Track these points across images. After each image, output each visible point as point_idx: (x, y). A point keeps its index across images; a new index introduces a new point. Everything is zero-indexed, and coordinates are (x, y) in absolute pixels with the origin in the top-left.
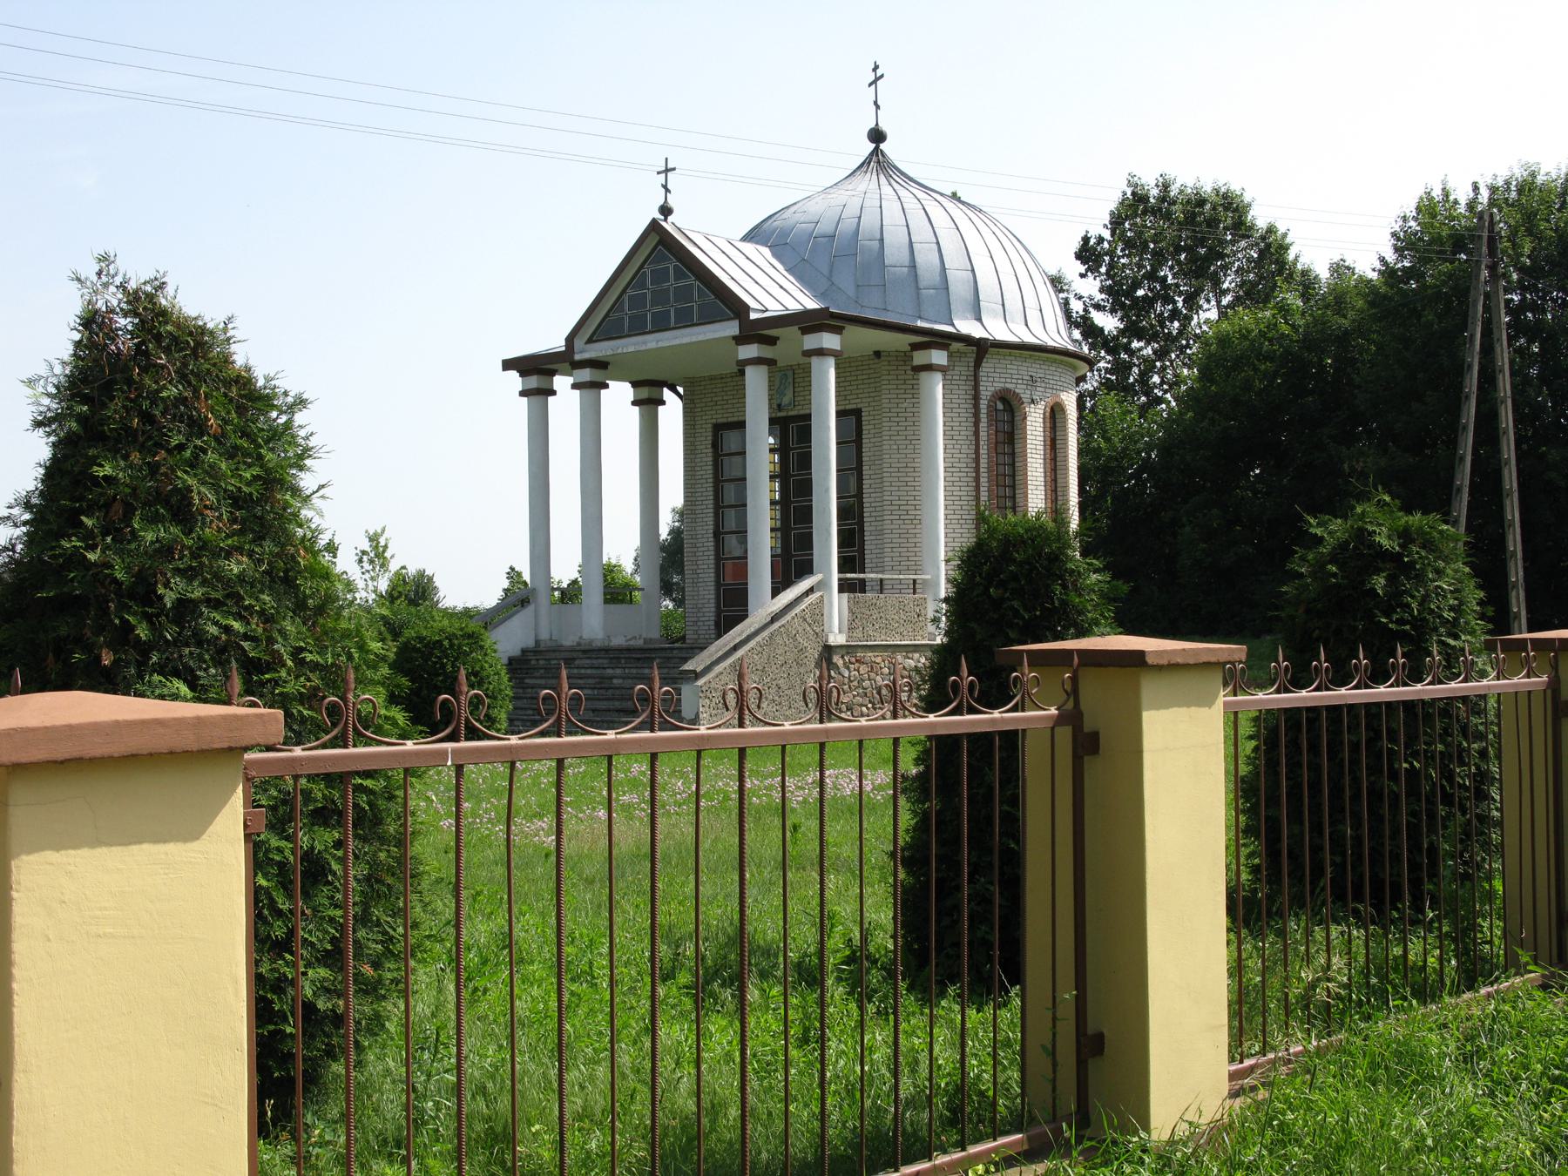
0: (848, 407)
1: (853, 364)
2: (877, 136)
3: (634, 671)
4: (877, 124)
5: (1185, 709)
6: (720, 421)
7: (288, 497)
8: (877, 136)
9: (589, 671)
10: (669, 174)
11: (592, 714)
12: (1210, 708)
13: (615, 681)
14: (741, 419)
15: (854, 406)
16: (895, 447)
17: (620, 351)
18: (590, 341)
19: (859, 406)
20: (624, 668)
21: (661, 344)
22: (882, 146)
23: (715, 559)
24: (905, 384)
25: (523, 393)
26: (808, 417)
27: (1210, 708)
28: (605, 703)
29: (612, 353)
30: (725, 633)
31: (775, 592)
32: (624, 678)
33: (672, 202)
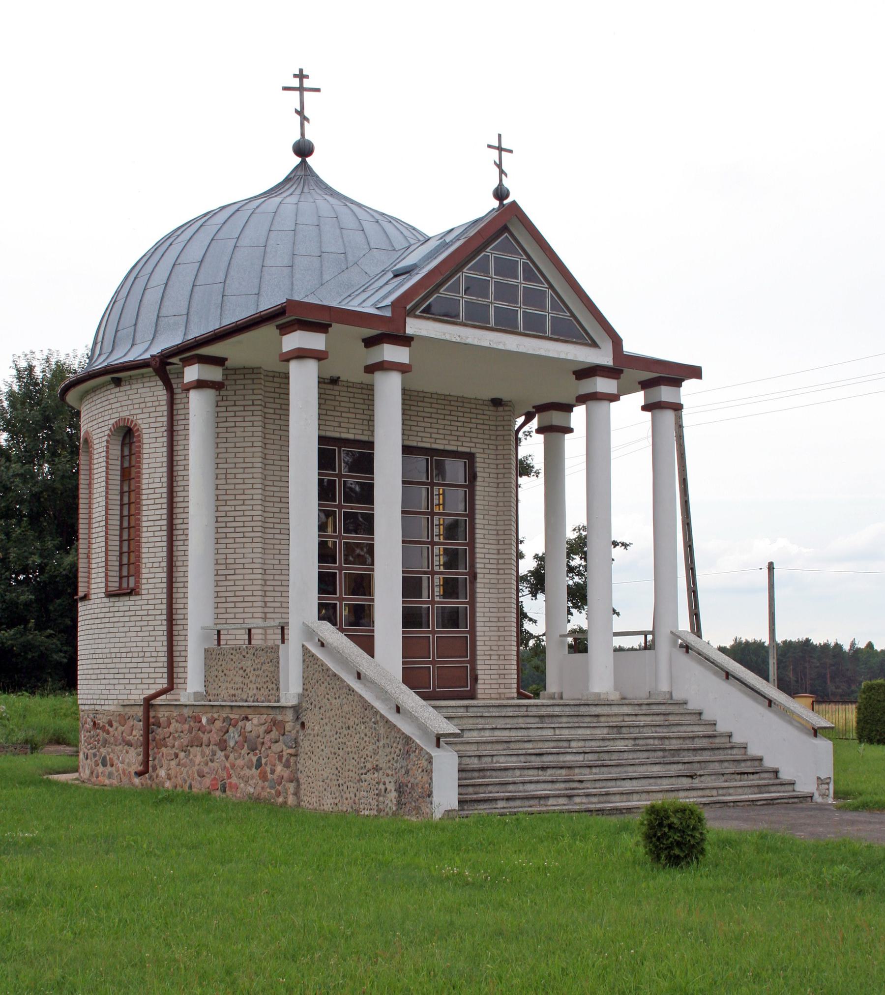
0: (461, 449)
2: (303, 149)
4: (303, 134)
5: (817, 640)
7: (56, 542)
8: (303, 149)
10: (298, 93)
12: (808, 641)
14: (371, 439)
15: (467, 450)
19: (473, 450)
22: (308, 160)
25: (645, 408)
26: (370, 445)
27: (808, 641)
30: (417, 693)
31: (367, 645)
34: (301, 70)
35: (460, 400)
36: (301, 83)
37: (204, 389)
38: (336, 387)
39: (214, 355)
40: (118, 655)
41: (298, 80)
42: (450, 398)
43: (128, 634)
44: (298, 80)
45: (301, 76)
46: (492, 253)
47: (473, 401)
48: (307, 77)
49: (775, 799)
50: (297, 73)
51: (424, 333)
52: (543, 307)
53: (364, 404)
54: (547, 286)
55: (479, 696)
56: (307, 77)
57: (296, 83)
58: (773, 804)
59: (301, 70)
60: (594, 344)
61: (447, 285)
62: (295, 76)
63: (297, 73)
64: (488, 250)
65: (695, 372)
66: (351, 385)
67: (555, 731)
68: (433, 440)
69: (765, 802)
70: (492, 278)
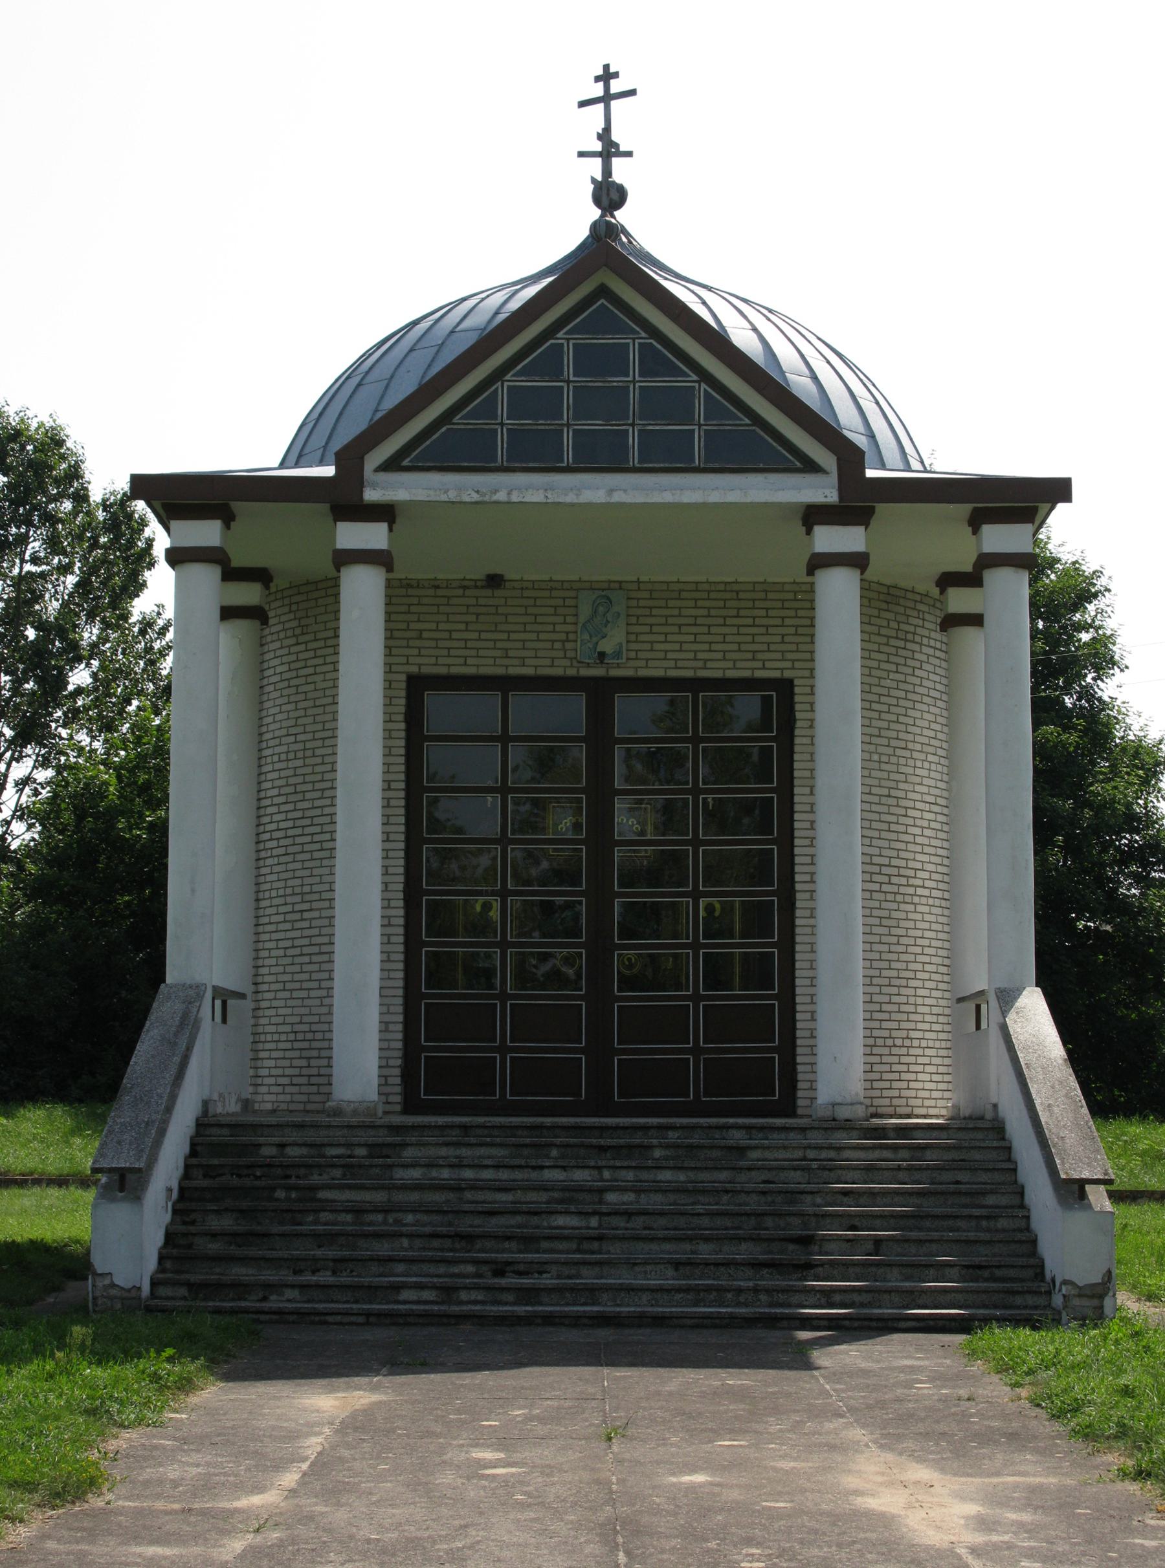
1: (771, 596)
3: (630, 1175)
6: (425, 670)
9: (488, 1174)
10: (614, 104)
11: (670, 1272)
13: (611, 1197)
15: (776, 674)
16: (876, 757)
17: (515, 498)
18: (392, 465)
19: (787, 674)
20: (599, 1168)
21: (617, 497)
23: (406, 943)
24: (420, 638)
28: (667, 1246)
29: (476, 497)
32: (638, 1191)
33: (621, 171)
34: (606, 67)
35: (758, 587)
36: (607, 88)
37: (231, 620)
38: (498, 593)
39: (997, 526)
40: (276, 1037)
41: (601, 84)
42: (736, 587)
43: (307, 1002)
44: (601, 84)
45: (607, 76)
46: (568, 339)
47: (787, 587)
48: (616, 75)
49: (681, 1317)
50: (612, 70)
51: (421, 495)
52: (688, 418)
53: (555, 614)
54: (695, 378)
55: (800, 1111)
56: (616, 75)
57: (598, 90)
58: (326, 1323)
59: (606, 67)
60: (810, 467)
61: (469, 409)
62: (598, 79)
63: (612, 70)
64: (560, 335)
65: (1059, 490)
66: (530, 585)
67: (600, 1173)
68: (700, 664)
69: (274, 1317)
70: (568, 382)
